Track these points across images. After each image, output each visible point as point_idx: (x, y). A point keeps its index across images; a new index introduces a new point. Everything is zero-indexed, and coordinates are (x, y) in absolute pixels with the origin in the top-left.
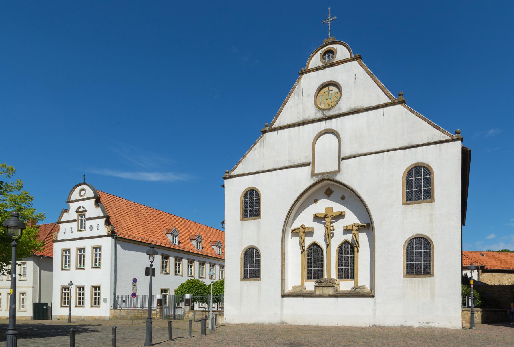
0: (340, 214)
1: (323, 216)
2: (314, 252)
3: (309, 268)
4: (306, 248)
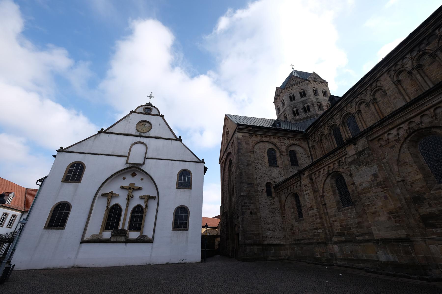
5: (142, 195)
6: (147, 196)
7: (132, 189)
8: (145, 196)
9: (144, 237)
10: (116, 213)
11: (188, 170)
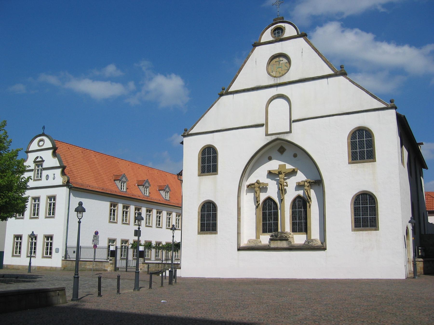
0: (293, 171)
4: (261, 202)
11: (365, 127)
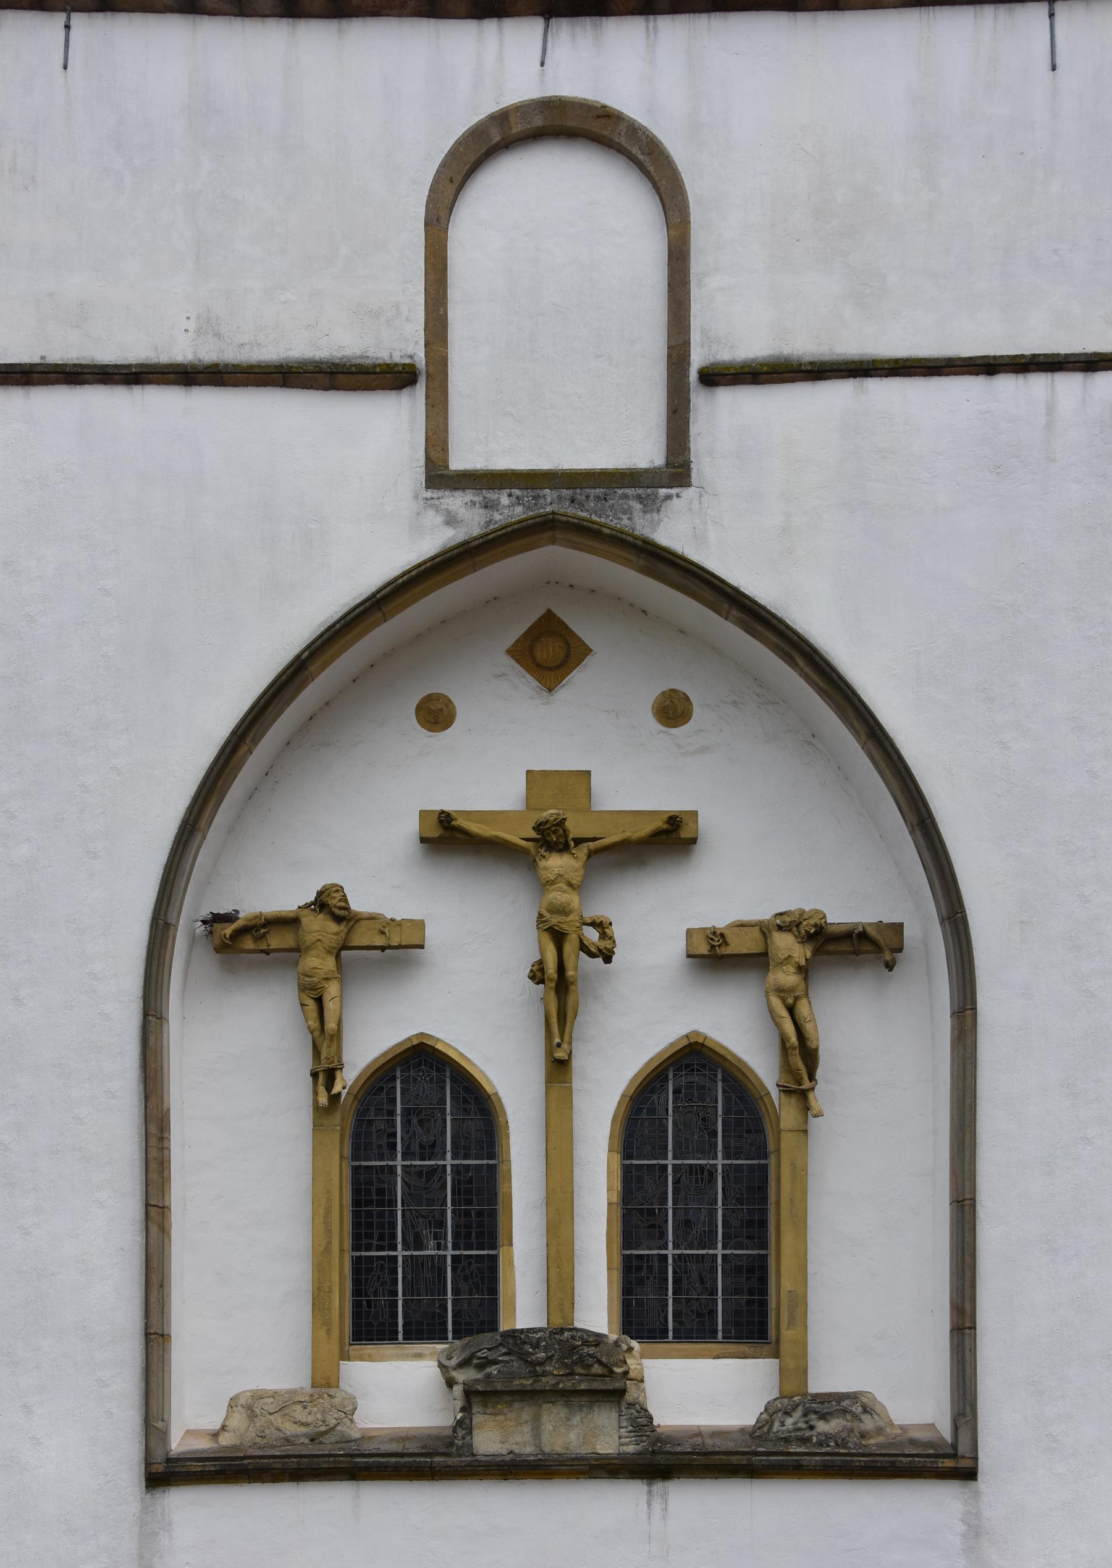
0: (658, 834)
1: (518, 834)
2: (415, 1120)
3: (368, 1248)
4: (350, 1076)
5: (720, 917)
6: (788, 923)
7: (579, 841)
8: (764, 929)
9: (844, 1411)
10: (432, 1149)
